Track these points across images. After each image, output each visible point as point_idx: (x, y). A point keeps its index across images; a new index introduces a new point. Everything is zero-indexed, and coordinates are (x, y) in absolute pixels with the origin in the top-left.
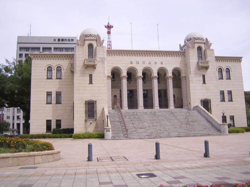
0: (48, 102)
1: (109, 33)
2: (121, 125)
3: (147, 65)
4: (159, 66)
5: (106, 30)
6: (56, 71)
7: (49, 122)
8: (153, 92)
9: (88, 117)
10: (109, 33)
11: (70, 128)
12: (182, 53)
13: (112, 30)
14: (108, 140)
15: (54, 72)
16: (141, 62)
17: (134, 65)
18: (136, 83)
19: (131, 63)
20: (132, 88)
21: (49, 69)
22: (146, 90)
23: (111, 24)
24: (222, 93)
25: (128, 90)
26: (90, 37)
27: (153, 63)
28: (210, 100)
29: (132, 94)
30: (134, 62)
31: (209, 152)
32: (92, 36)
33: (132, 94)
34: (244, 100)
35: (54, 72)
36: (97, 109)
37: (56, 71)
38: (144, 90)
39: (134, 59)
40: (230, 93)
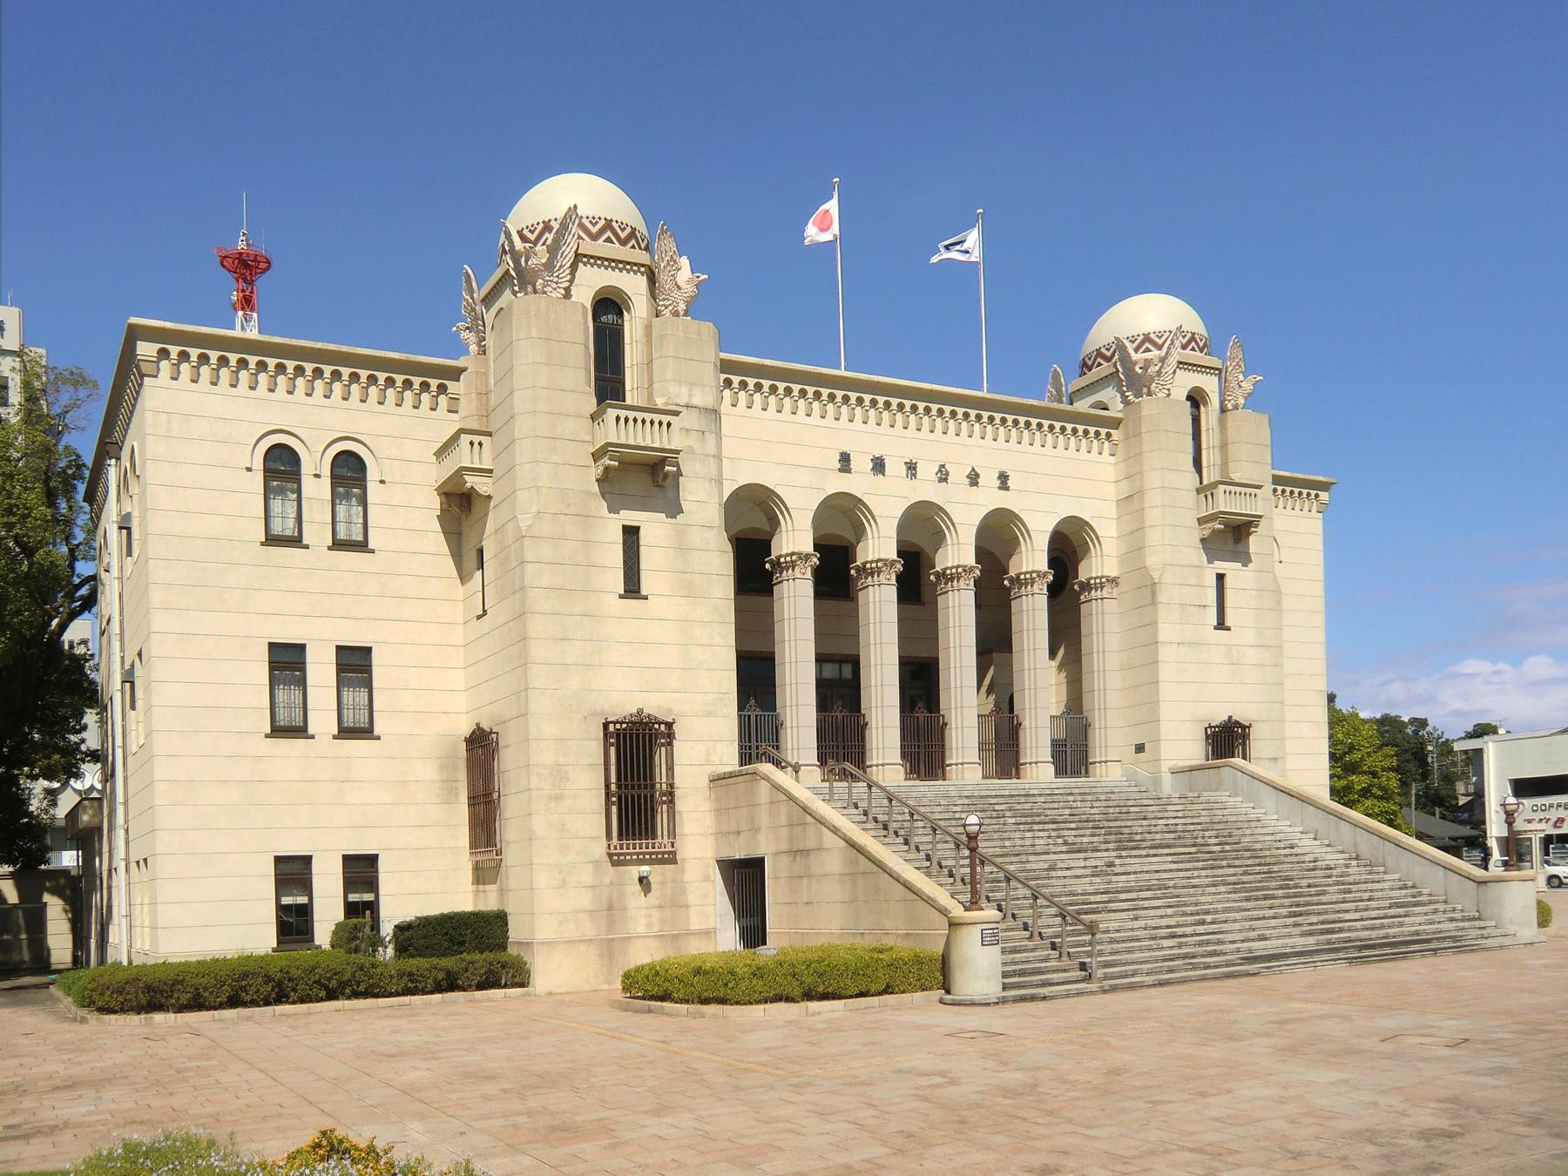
0: (283, 718)
2: (1296, 925)
3: (925, 489)
4: (989, 499)
6: (326, 482)
7: (293, 872)
8: (1015, 676)
9: (620, 837)
14: (973, 1004)
15: (316, 487)
16: (895, 467)
17: (858, 483)
18: (854, 616)
21: (281, 466)
22: (847, 662)
24: (287, 662)
26: (608, 240)
27: (958, 475)
28: (669, 725)
29: (840, 691)
31: (180, 964)
33: (840, 691)
34: (1324, 748)
35: (316, 487)
36: (677, 782)
37: (260, 477)
38: (821, 659)
40: (354, 664)
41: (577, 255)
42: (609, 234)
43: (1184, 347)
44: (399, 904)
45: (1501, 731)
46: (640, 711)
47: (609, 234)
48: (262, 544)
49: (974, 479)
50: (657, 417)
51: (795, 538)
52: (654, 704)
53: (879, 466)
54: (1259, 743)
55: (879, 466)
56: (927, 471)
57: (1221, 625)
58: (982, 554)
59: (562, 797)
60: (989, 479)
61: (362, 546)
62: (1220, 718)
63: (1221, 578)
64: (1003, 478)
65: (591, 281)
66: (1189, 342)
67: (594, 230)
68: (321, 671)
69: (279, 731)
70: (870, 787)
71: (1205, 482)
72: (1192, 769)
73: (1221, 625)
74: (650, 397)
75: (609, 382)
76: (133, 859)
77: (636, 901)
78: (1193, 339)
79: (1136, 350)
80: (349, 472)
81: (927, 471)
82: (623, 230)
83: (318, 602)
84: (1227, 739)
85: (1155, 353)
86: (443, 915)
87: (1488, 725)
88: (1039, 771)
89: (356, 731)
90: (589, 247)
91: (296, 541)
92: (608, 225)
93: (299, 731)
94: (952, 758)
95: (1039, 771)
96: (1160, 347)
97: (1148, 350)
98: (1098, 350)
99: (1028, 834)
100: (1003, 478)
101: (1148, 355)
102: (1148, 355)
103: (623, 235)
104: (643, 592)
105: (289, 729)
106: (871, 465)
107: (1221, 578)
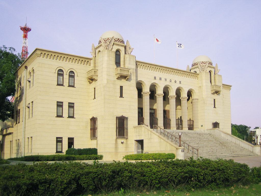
1: (25, 37)
3: (167, 83)
5: (22, 33)
7: (59, 140)
10: (25, 37)
11: (82, 148)
12: (191, 73)
13: (29, 33)
15: (66, 77)
19: (155, 78)
20: (141, 107)
21: (60, 73)
23: (29, 26)
24: (60, 105)
25: (138, 108)
26: (118, 42)
27: (173, 81)
30: (158, 78)
32: (120, 41)
35: (66, 77)
39: (158, 74)
40: (71, 106)
41: (114, 44)
42: (118, 41)
43: (209, 64)
44: (77, 146)
45: (260, 128)
46: (122, 116)
47: (118, 41)
48: (57, 85)
49: (175, 82)
50: (125, 69)
51: (146, 90)
52: (125, 115)
53: (160, 79)
54: (220, 126)
55: (160, 79)
56: (178, 82)
57: (215, 107)
58: (176, 94)
59: (107, 129)
60: (178, 82)
61: (73, 86)
62: (214, 122)
63: (121, 87)
64: (180, 82)
65: (115, 48)
66: (209, 63)
67: (116, 40)
68: (66, 106)
69: (58, 116)
70: (160, 129)
71: (212, 85)
72: (210, 129)
73: (215, 107)
74: (124, 66)
75: (118, 63)
76: (27, 137)
77: (120, 145)
78: (210, 63)
79: (201, 64)
80: (72, 75)
81: (168, 80)
82: (121, 40)
83: (66, 95)
84: (216, 125)
85: (204, 65)
86: (43, 156)
87: (257, 127)
88: (185, 129)
89: (71, 117)
90: (115, 43)
91: (62, 85)
92: (118, 39)
93: (61, 116)
94: (172, 126)
95: (185, 129)
96: (205, 64)
97: (203, 64)
98: (195, 63)
99: (186, 138)
100: (180, 82)
101: (203, 65)
102: (203, 65)
103: (121, 41)
104: (123, 97)
105: (59, 116)
106: (159, 79)
107: (121, 87)
